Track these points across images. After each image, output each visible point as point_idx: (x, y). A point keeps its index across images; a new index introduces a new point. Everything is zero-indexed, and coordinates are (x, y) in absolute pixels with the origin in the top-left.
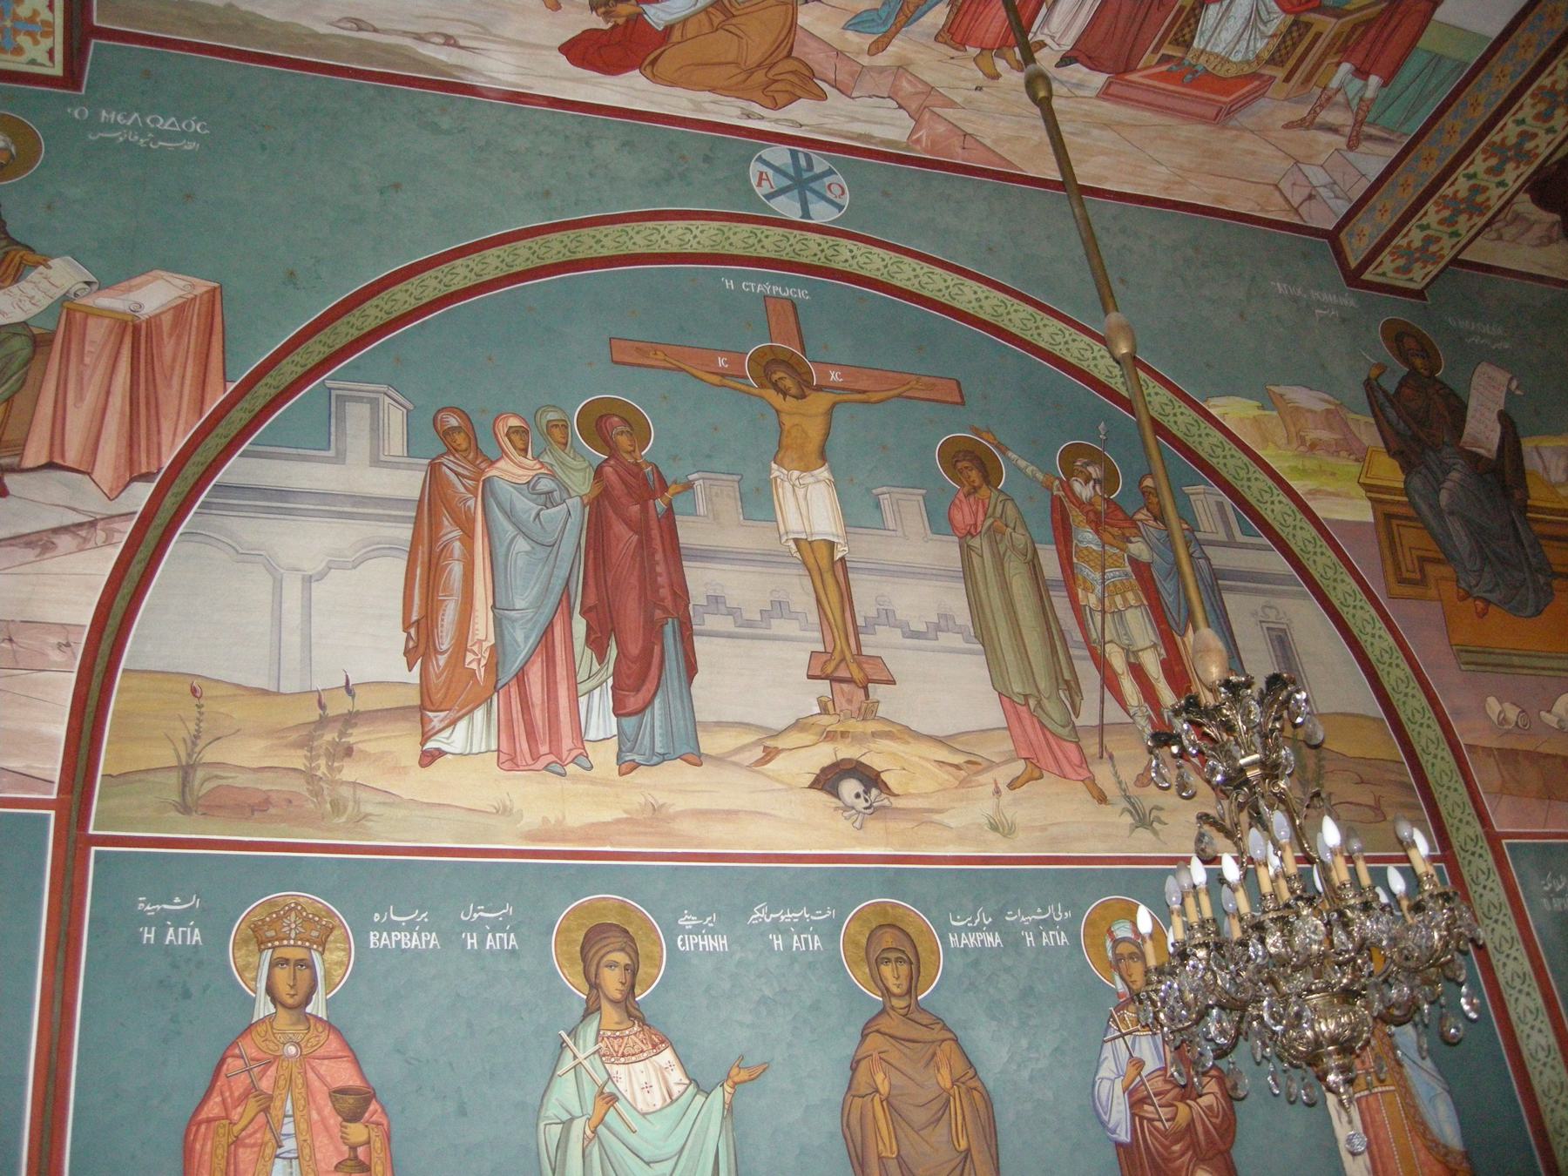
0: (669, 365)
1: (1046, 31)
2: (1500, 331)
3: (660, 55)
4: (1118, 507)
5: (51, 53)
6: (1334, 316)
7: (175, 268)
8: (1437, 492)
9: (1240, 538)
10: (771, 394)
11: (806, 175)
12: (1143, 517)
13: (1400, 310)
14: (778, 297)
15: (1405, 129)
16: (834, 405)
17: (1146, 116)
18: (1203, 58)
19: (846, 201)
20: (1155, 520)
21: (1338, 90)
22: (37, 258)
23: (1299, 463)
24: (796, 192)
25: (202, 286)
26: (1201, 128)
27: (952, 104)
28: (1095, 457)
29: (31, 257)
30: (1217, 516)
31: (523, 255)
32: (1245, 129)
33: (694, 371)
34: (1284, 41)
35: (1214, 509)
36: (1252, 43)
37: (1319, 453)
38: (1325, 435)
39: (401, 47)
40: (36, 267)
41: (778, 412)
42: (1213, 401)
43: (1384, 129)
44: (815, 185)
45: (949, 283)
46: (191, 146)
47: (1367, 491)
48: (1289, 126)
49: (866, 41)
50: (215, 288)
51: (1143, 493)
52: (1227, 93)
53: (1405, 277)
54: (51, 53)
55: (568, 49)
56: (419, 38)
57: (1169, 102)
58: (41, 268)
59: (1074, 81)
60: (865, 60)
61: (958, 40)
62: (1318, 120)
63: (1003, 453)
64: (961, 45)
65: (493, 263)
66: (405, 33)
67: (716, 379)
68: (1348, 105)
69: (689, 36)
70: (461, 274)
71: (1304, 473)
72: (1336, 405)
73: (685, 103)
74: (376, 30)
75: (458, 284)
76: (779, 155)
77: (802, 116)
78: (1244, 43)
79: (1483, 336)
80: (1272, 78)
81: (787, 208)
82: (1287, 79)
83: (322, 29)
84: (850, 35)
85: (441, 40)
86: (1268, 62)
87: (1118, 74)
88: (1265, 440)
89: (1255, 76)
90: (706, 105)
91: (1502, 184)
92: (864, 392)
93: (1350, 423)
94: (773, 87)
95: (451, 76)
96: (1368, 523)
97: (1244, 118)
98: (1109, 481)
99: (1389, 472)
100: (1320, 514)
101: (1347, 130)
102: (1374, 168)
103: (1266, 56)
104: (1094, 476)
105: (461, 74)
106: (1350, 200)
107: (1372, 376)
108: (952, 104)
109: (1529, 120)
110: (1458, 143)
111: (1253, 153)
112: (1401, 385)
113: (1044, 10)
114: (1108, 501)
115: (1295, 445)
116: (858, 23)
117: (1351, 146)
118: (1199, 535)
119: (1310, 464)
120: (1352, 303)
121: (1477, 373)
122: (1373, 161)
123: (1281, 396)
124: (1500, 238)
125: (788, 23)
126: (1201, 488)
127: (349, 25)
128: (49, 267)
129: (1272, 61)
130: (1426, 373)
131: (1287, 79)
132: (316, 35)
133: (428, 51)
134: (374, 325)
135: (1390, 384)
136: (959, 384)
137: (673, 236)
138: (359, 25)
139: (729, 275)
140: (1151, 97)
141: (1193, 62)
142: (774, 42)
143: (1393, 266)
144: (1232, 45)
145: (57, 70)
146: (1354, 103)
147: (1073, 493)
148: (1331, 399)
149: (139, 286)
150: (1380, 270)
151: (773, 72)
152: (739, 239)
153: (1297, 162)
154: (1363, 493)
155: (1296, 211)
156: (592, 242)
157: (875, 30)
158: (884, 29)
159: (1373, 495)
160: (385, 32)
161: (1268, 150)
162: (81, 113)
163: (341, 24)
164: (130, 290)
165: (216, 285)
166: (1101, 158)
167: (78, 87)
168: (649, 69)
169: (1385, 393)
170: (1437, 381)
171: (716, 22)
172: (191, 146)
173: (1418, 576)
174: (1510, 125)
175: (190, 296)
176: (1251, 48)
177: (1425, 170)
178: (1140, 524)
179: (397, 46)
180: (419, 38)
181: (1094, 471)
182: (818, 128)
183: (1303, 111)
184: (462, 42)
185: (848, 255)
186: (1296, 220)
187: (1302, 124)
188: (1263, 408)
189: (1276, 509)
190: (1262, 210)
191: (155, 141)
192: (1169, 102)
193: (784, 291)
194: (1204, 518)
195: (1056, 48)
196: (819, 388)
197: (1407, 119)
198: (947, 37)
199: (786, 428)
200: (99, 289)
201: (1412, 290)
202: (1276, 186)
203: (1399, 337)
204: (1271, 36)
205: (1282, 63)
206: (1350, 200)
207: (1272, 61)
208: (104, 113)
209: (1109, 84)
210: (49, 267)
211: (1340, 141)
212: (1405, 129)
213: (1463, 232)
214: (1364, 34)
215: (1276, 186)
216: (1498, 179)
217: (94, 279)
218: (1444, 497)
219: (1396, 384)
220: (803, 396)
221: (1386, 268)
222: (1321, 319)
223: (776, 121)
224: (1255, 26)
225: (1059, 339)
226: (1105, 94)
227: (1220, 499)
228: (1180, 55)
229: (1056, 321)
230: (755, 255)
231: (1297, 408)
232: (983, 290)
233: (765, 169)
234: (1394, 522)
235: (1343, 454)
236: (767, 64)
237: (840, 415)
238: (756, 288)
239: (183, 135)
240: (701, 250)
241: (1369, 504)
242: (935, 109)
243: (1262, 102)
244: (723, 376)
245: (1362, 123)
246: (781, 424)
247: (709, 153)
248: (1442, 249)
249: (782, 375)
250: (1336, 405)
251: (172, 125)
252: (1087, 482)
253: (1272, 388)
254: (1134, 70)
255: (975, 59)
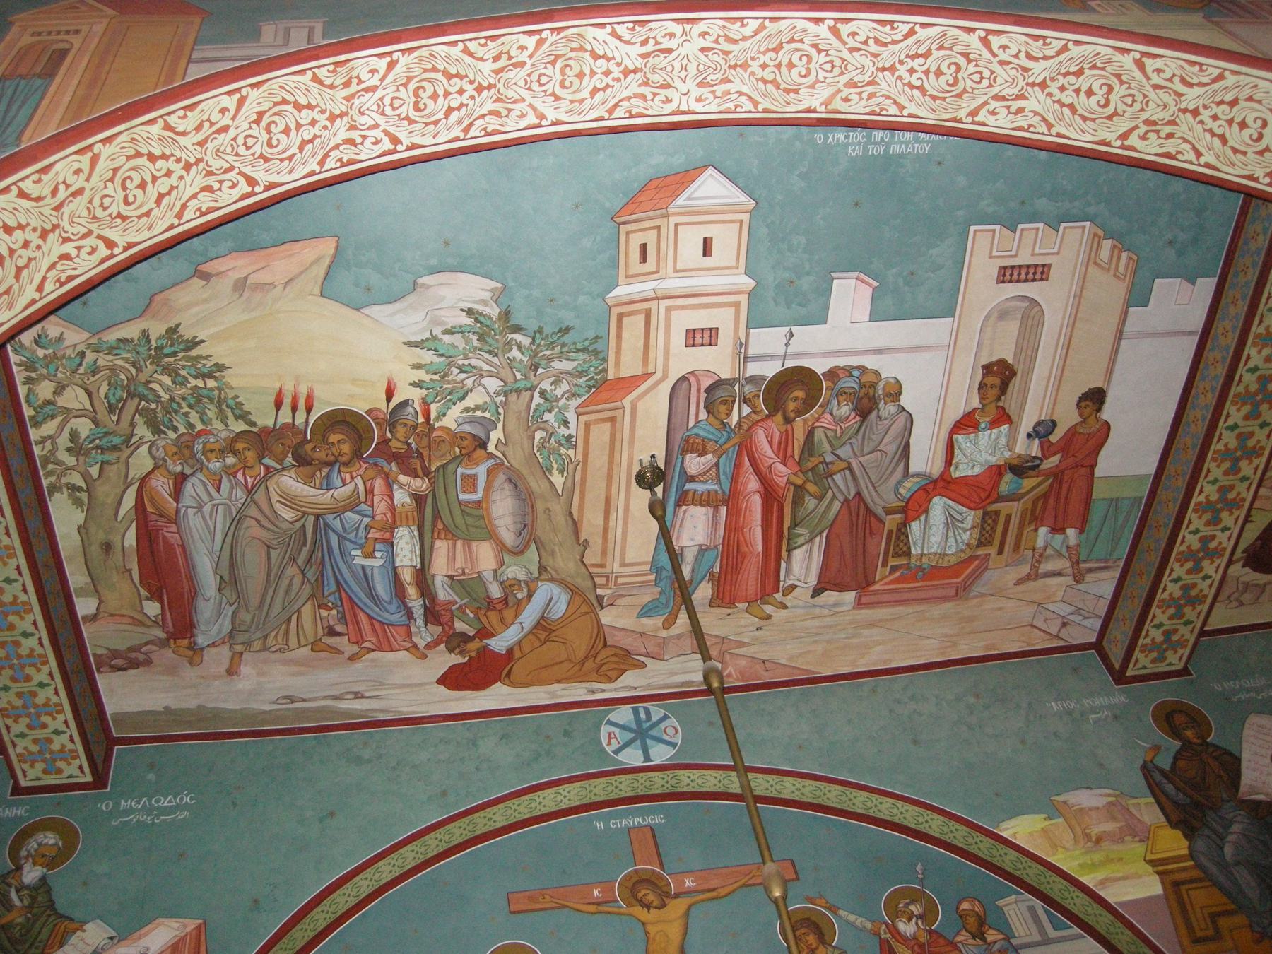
0: (554, 905)
1: (792, 577)
2: (1263, 681)
3: (511, 668)
4: (941, 936)
5: (81, 768)
6: (1107, 716)
7: (171, 914)
8: (1222, 848)
9: (1052, 934)
10: (638, 911)
11: (646, 725)
12: (963, 938)
13: (1165, 692)
14: (640, 827)
15: (1115, 556)
16: (690, 907)
17: (900, 610)
18: (925, 560)
19: (679, 739)
20: (974, 938)
21: (1046, 547)
22: (77, 925)
23: (1087, 859)
24: (638, 742)
25: (191, 924)
26: (949, 605)
27: (743, 644)
28: (916, 896)
29: (72, 926)
30: (1030, 921)
31: (433, 844)
32: (983, 595)
33: (575, 906)
34: (983, 528)
35: (1027, 915)
36: (958, 537)
37: (1105, 844)
38: (1109, 826)
39: (327, 707)
40: (75, 932)
41: (643, 924)
42: (1004, 825)
43: (1098, 561)
44: (653, 732)
45: (771, 782)
46: (183, 815)
47: (1154, 866)
48: (1018, 583)
49: (659, 621)
50: (200, 925)
51: (961, 916)
52: (957, 576)
53: (1164, 664)
54: (81, 768)
55: (441, 681)
56: (336, 698)
57: (913, 595)
58: (79, 933)
59: (831, 603)
60: (664, 634)
61: (727, 601)
62: (1040, 571)
63: (835, 913)
64: (731, 603)
65: (410, 855)
66: (325, 698)
67: (592, 908)
68: (1060, 555)
69: (527, 651)
70: (386, 870)
71: (1093, 867)
72: (1116, 796)
73: (542, 695)
74: (304, 700)
75: (386, 877)
76: (624, 714)
77: (631, 682)
78: (951, 540)
79: (1248, 690)
80: (987, 556)
81: (632, 757)
82: (1000, 552)
83: (267, 708)
84: (644, 620)
85: (352, 696)
86: (978, 546)
87: (863, 588)
88: (1054, 846)
89: (972, 559)
90: (558, 693)
91: (1205, 577)
92: (714, 890)
93: (1132, 809)
94: (604, 668)
95: (367, 717)
96: (1158, 896)
97: (977, 589)
98: (928, 916)
99: (1173, 843)
100: (1111, 899)
101: (1069, 571)
102: (1108, 589)
103: (974, 542)
104: (916, 913)
105: (374, 715)
106: (1099, 617)
107: (1148, 759)
108: (743, 644)
109: (1202, 528)
110: (1155, 559)
111: (1000, 609)
112: (1176, 758)
113: (783, 565)
114: (930, 932)
115: (1082, 843)
116: (647, 612)
117: (1079, 578)
118: (1014, 941)
119: (1097, 857)
120: (1123, 699)
121: (1246, 725)
122: (1104, 585)
123: (1065, 803)
124: (1242, 604)
125: (596, 625)
126: (1013, 898)
127: (285, 701)
128: (84, 931)
129: (980, 544)
130: (1199, 741)
131: (1000, 552)
132: (265, 712)
133: (344, 705)
134: (303, 943)
135: (1164, 762)
136: (793, 862)
137: (547, 801)
138: (292, 700)
139: (598, 818)
140: (897, 596)
141: (918, 563)
142: (591, 637)
143: (1181, 632)
144: (943, 544)
145: (88, 778)
146: (1064, 551)
147: (899, 933)
148: (1111, 792)
149: (146, 934)
150: (1140, 665)
151: (598, 660)
152: (599, 789)
153: (1039, 605)
154: (1150, 869)
155: (1058, 637)
156: (485, 821)
157: (661, 612)
158: (668, 610)
159: (1161, 868)
160: (310, 700)
161: (1010, 604)
162: (107, 805)
163: (279, 701)
164: (140, 938)
165: (201, 921)
166: (879, 648)
167: (105, 786)
168: (507, 680)
169: (1161, 771)
170: (1208, 745)
171: (542, 638)
172: (183, 815)
173: (1211, 932)
174: (1188, 537)
175: (183, 934)
176: (960, 541)
177: (1140, 586)
178: (960, 945)
179: (323, 707)
180: (336, 698)
181: (916, 909)
182: (649, 687)
183: (1026, 569)
184: (367, 694)
185: (688, 781)
186: (1061, 643)
187: (1028, 578)
188: (1049, 818)
189: (1077, 902)
190: (1028, 645)
191: (158, 816)
192: (913, 595)
193: (644, 820)
194: (1018, 924)
195: (806, 586)
196: (677, 895)
197: (1113, 550)
198: (719, 602)
199: (651, 936)
200: (119, 941)
201: (1176, 671)
202: (1032, 626)
203: (1169, 717)
204: (971, 529)
205: (990, 543)
206: (1099, 617)
207: (980, 544)
208: (123, 802)
209: (859, 598)
210: (84, 931)
211: (1069, 580)
212: (1115, 556)
213: (1194, 619)
214: (1044, 507)
215: (1032, 626)
216: (1202, 575)
217: (115, 934)
218: (1228, 850)
219: (1170, 760)
220: (664, 905)
221: (1142, 662)
222: (1095, 722)
223: (615, 690)
224: (954, 526)
225: (869, 804)
226: (859, 604)
227: (1030, 903)
228: (905, 562)
229: (861, 793)
230: (616, 797)
231: (1081, 810)
232: (798, 782)
233: (612, 729)
234: (1183, 888)
235: (1128, 838)
236: (591, 654)
237: (695, 912)
238: (621, 823)
239: (178, 807)
240: (573, 804)
241: (1157, 877)
242: (732, 651)
243: (987, 574)
244: (598, 904)
245: (1078, 563)
246: (647, 933)
247: (567, 728)
248: (1183, 636)
249: (644, 892)
250: (1116, 796)
251: (170, 802)
252: (910, 920)
253: (1057, 798)
254: (874, 583)
255: (746, 611)
